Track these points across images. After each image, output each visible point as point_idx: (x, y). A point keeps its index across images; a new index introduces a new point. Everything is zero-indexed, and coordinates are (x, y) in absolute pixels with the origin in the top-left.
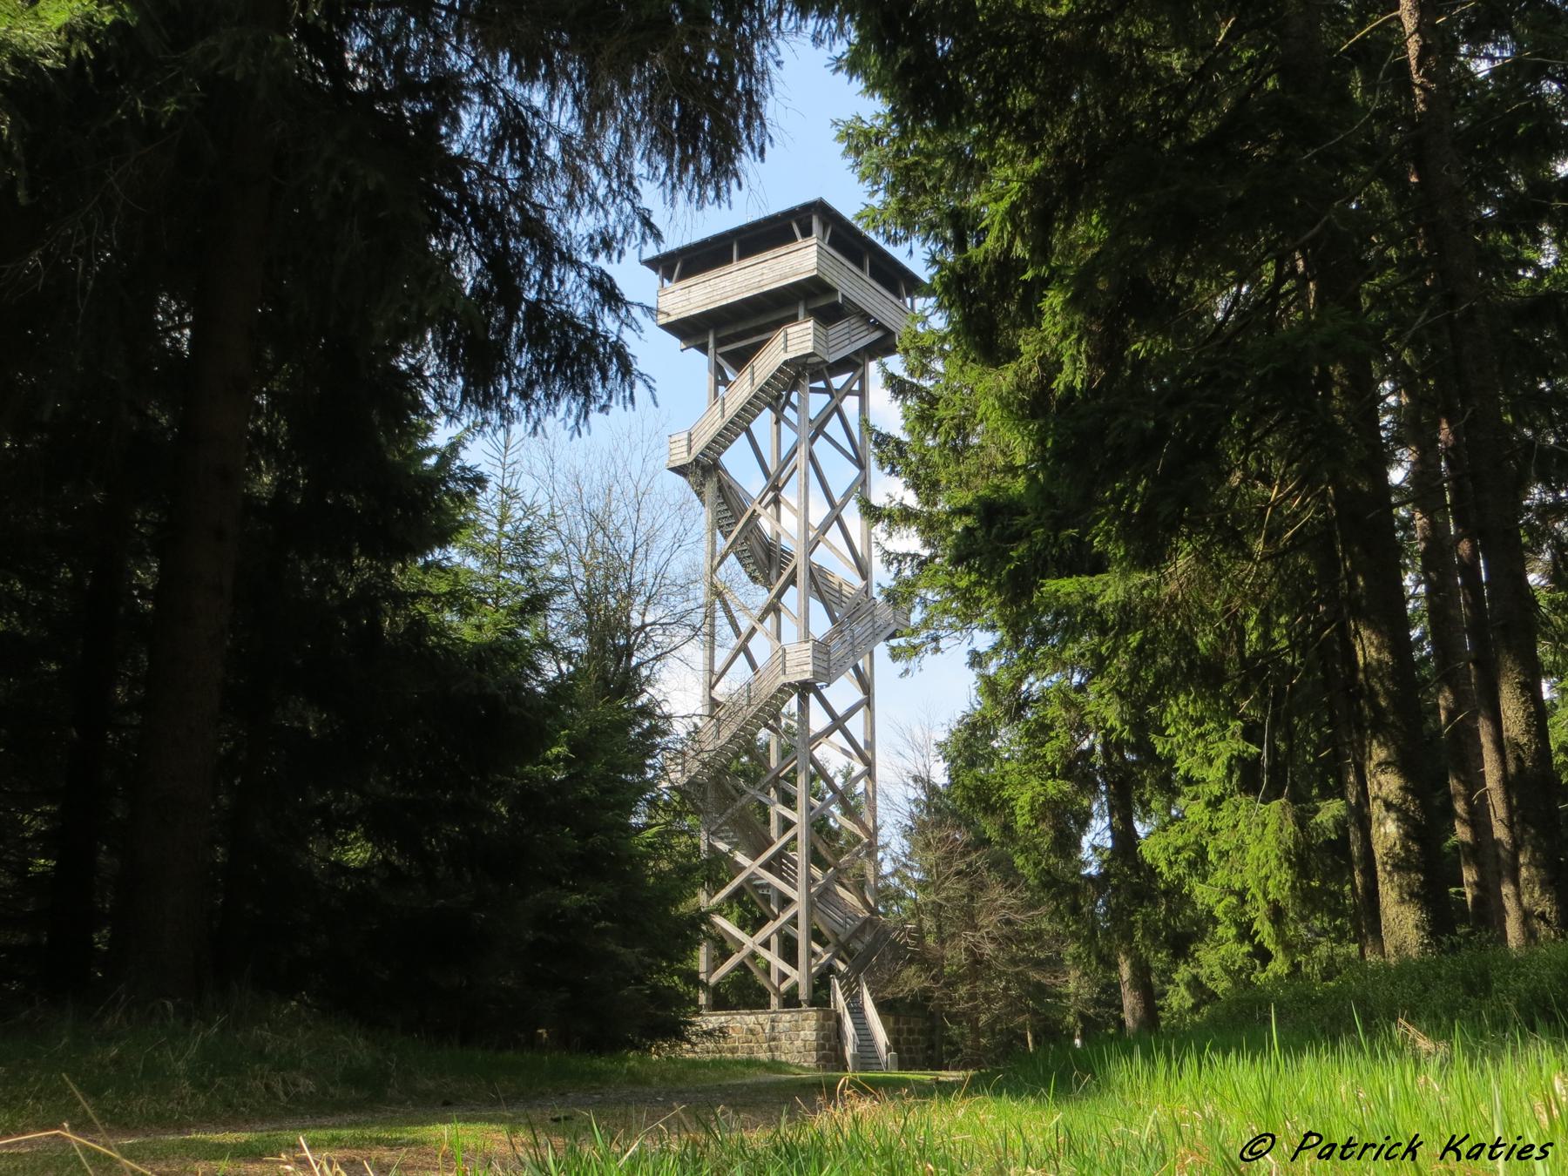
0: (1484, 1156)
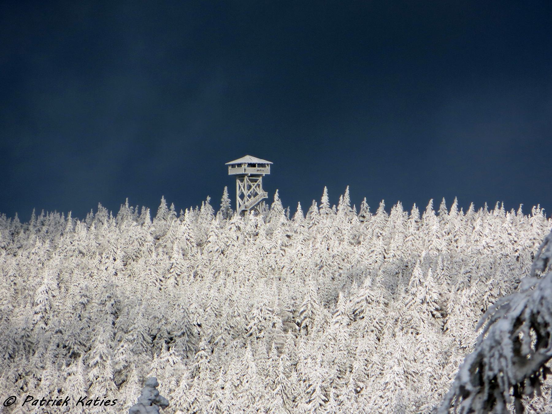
0: (92, 405)
